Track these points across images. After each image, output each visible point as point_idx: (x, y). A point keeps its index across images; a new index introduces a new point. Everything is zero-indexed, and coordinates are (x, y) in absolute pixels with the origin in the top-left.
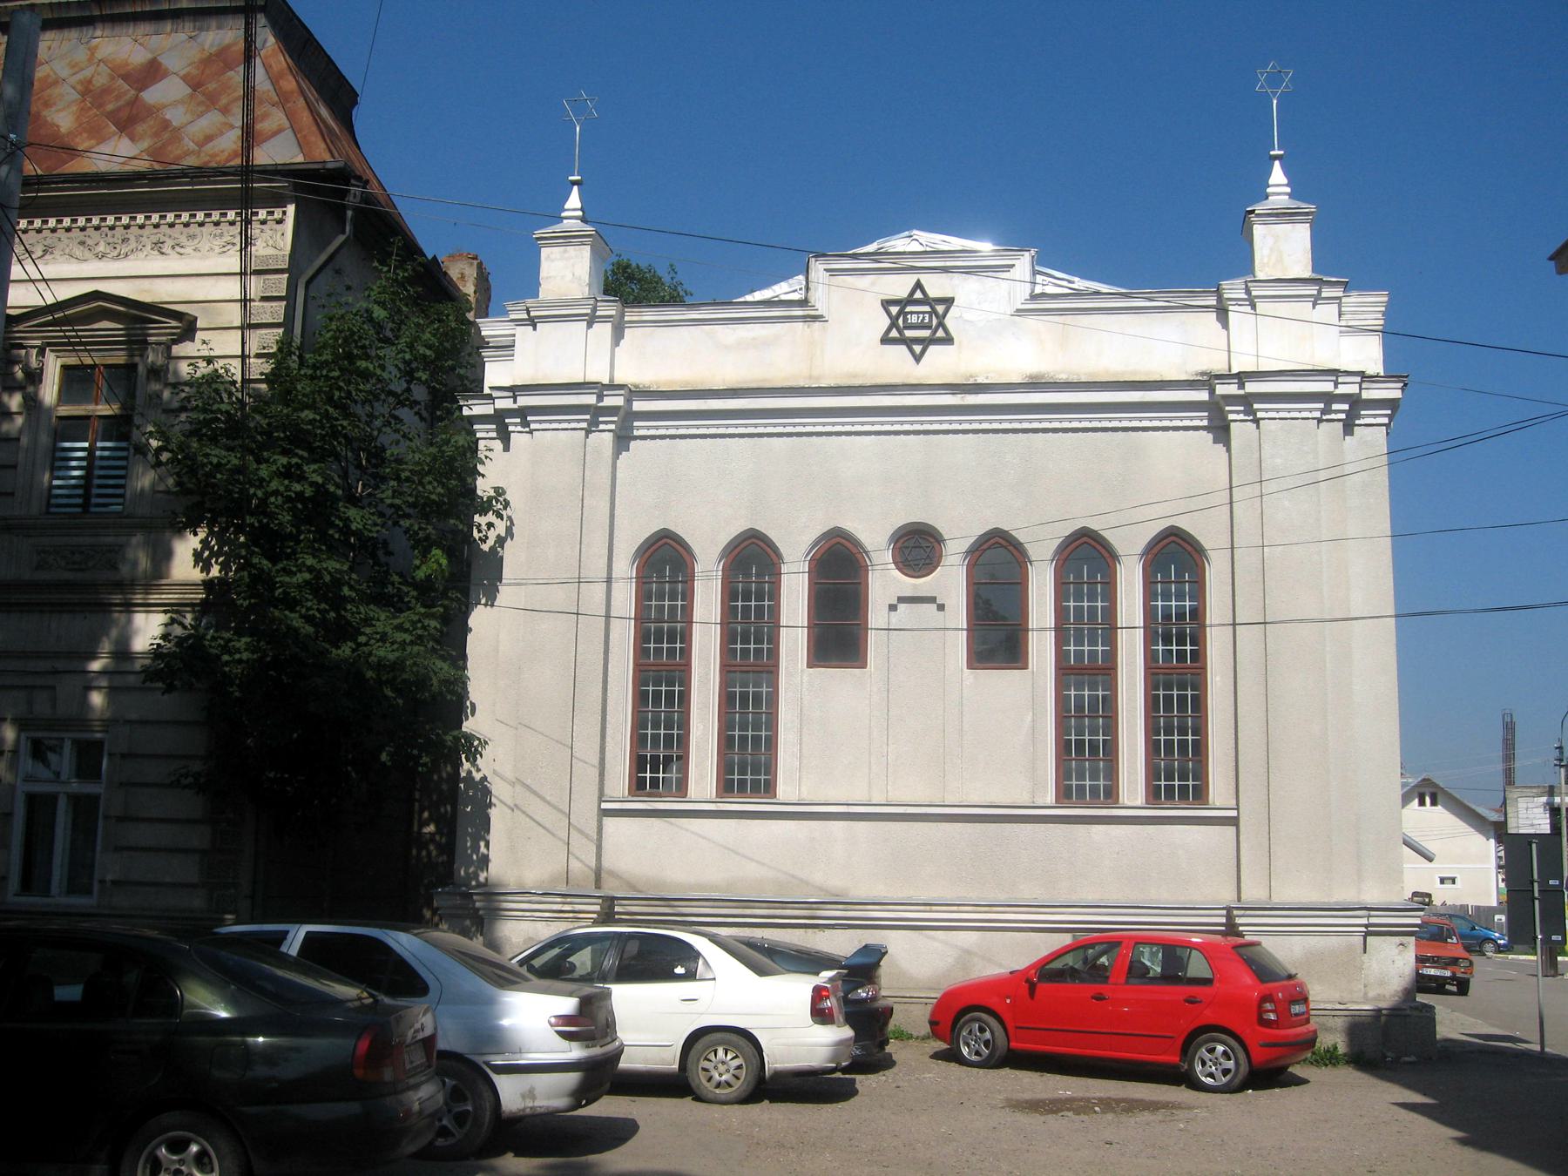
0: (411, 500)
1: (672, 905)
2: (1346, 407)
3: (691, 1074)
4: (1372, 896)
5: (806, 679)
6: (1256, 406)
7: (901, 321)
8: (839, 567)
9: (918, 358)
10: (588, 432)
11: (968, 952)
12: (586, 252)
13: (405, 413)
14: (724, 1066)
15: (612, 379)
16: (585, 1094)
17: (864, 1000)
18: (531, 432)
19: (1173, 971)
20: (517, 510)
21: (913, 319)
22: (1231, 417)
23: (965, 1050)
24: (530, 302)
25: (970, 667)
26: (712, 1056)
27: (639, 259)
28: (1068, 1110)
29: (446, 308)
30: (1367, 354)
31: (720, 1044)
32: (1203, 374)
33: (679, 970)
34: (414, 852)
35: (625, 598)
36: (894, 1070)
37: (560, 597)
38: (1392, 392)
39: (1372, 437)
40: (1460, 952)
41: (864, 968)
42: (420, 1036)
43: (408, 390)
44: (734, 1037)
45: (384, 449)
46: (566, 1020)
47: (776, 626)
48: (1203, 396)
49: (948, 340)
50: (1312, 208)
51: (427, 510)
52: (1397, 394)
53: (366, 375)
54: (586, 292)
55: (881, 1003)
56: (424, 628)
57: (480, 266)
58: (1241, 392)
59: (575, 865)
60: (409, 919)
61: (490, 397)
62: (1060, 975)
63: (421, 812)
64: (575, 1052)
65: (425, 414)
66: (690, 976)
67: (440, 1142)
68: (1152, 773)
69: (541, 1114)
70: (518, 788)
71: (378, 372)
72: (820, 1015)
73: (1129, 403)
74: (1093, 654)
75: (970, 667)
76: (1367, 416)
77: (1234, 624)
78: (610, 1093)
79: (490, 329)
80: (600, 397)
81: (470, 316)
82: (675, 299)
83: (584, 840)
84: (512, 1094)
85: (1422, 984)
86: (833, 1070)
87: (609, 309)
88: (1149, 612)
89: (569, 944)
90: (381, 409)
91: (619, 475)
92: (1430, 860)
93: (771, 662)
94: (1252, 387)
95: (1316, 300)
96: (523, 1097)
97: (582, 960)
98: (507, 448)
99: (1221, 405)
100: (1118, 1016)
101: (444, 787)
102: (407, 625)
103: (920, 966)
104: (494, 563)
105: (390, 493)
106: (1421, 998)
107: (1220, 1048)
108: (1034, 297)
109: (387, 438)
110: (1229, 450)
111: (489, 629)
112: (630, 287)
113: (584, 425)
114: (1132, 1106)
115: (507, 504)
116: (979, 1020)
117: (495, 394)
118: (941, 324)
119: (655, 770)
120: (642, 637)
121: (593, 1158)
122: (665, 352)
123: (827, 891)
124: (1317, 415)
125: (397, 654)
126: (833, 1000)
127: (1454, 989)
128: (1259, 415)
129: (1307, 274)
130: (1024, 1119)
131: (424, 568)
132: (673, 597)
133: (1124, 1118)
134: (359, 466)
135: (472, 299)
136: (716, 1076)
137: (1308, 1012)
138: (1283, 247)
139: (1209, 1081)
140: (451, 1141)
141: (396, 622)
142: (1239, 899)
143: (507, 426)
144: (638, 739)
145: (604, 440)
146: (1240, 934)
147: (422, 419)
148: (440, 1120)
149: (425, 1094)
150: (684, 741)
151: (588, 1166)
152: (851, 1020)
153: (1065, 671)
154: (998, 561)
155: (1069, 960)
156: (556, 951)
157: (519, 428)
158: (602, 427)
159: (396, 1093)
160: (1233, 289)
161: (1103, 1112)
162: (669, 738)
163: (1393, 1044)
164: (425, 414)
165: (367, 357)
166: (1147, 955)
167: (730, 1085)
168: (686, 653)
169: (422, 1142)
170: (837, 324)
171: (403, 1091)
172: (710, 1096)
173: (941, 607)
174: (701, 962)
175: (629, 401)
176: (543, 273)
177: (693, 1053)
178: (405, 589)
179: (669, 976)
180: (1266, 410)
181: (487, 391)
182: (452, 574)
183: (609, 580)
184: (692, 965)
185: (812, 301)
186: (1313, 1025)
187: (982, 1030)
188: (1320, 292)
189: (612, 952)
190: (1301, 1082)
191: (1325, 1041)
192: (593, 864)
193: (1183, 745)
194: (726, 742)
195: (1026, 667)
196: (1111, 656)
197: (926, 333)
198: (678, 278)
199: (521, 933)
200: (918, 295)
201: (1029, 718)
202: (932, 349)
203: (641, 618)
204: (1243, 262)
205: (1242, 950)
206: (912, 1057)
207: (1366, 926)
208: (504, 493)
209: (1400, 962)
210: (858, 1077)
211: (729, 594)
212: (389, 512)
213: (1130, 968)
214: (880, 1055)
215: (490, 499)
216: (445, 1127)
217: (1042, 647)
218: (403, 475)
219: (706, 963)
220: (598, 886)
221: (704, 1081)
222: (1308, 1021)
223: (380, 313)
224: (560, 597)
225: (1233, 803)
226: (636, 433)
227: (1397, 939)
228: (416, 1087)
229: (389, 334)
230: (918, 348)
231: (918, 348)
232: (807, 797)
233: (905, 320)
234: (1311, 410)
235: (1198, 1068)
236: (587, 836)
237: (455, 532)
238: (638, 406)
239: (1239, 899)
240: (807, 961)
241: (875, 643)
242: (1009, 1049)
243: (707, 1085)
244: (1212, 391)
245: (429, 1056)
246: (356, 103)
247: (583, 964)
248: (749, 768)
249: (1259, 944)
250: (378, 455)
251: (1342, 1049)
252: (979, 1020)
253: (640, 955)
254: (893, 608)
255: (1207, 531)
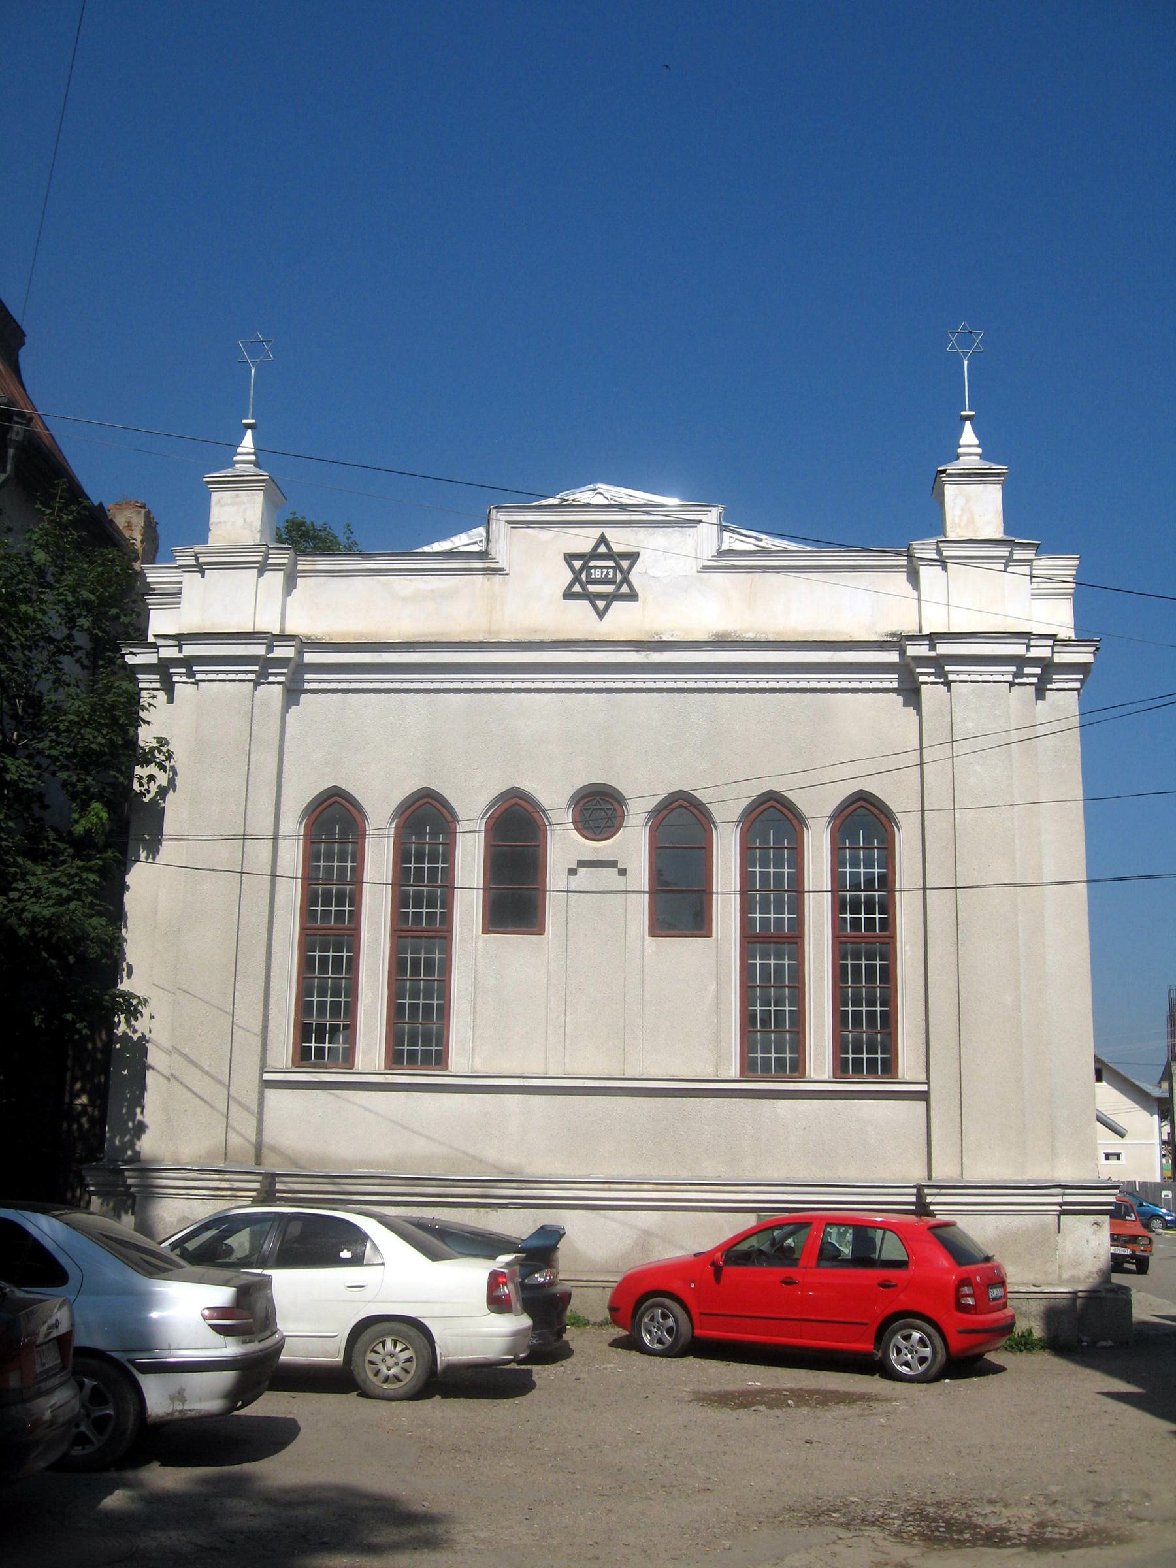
0: (69, 750)
1: (339, 1184)
2: (1038, 671)
3: (357, 1371)
4: (1066, 1173)
5: (480, 944)
6: (947, 668)
7: (584, 576)
8: (516, 831)
9: (601, 614)
10: (257, 684)
11: (647, 1233)
12: (259, 497)
13: (67, 662)
14: (392, 1359)
15: (282, 630)
16: (242, 1393)
17: (541, 1286)
18: (196, 683)
19: (864, 1256)
20: (179, 761)
21: (597, 574)
22: (922, 679)
23: (647, 1339)
24: (198, 548)
25: (653, 933)
26: (379, 1348)
27: (314, 517)
28: (760, 1403)
29: (112, 553)
30: (1059, 617)
31: (388, 1335)
32: (893, 635)
33: (346, 1254)
34: (65, 1125)
35: (292, 856)
36: (573, 1359)
37: (224, 854)
38: (1084, 656)
39: (1064, 701)
40: (1139, 1230)
41: (541, 1250)
42: (55, 1334)
43: (70, 637)
44: (404, 1328)
45: (41, 699)
46: (221, 1312)
47: (449, 887)
48: (894, 657)
49: (633, 596)
50: (1004, 469)
51: (87, 760)
52: (1089, 658)
53: (26, 620)
54: (256, 538)
55: (559, 1289)
56: (82, 882)
57: (148, 515)
58: (933, 654)
59: (235, 1140)
60: (57, 1195)
61: (153, 645)
62: (746, 1258)
63: (74, 1082)
64: (230, 1349)
65: (86, 662)
66: (357, 1260)
67: (77, 1451)
68: (840, 1045)
69: (193, 1419)
70: (175, 1056)
71: (39, 616)
72: (497, 1303)
73: (822, 663)
74: (779, 922)
75: (653, 933)
76: (1059, 681)
77: (925, 889)
78: (269, 1389)
79: (156, 575)
80: (270, 648)
81: (137, 566)
82: (350, 550)
83: (245, 1114)
84: (158, 1397)
85: (1117, 1264)
86: (509, 1362)
87: (281, 557)
88: (837, 878)
89: (225, 1225)
90: (40, 657)
91: (287, 730)
92: (1122, 1136)
93: (352, 926)
94: (943, 649)
95: (1008, 561)
96: (172, 1399)
97: (240, 1242)
98: (170, 700)
99: (913, 668)
100: (816, 1302)
101: (99, 1056)
102: (64, 879)
103: (597, 1248)
104: (155, 815)
105: (47, 743)
106: (1117, 1279)
107: (916, 1335)
108: (721, 553)
109: (44, 685)
110: (919, 713)
111: (147, 885)
112: (302, 538)
113: (253, 677)
114: (827, 1398)
115: (170, 756)
116: (660, 1305)
117: (160, 642)
118: (625, 580)
119: (320, 1040)
120: (310, 899)
121: (248, 1467)
122: (337, 604)
123: (502, 1171)
124: (1009, 678)
125: (52, 910)
126: (511, 1286)
127: (1134, 1267)
128: (951, 677)
129: (999, 535)
130: (715, 1415)
131: (83, 821)
132: (342, 859)
133: (819, 1412)
134: (15, 716)
135: (138, 546)
136: (384, 1370)
137: (1005, 1296)
138: (974, 509)
139: (904, 1370)
140: (89, 1449)
141: (50, 876)
142: (930, 1178)
143: (171, 675)
144: (304, 1007)
145: (273, 693)
146: (932, 1214)
147: (83, 667)
148: (77, 1426)
149: (58, 1401)
150: (351, 1009)
151: (246, 1479)
152: (529, 1307)
153: (751, 940)
154: (681, 827)
155: (753, 1242)
156: (211, 1233)
157: (184, 679)
158: (271, 679)
159: (24, 1401)
160: (925, 548)
161: (797, 1406)
162: (336, 1006)
163: (1091, 1328)
164: (86, 662)
165: (28, 600)
166: (834, 1236)
167: (399, 1380)
168: (355, 916)
169: (55, 1455)
170: (520, 576)
171: (31, 1399)
172: (378, 1392)
173: (623, 872)
174: (368, 1245)
175: (300, 653)
176: (213, 519)
177: (358, 1345)
178: (61, 846)
179: (330, 1259)
180: (958, 673)
181: (151, 639)
182: (111, 831)
183: (276, 838)
184: (360, 1248)
185: (492, 552)
186: (1009, 1311)
187: (665, 1316)
188: (1011, 553)
189: (273, 1234)
190: (998, 1369)
191: (1021, 1326)
192: (253, 1137)
193: (871, 1015)
194: (396, 1011)
195: (709, 935)
196: (798, 924)
197: (610, 589)
198: (354, 538)
199: (178, 1213)
200: (602, 549)
201: (714, 987)
202: (616, 604)
203: (309, 878)
204: (935, 523)
205: (938, 1231)
206: (589, 1343)
207: (1060, 1204)
208: (167, 743)
209: (1094, 1243)
210: (536, 1369)
211: (402, 855)
212: (45, 763)
213: (821, 1250)
214: (557, 1344)
215: (152, 749)
216: (82, 1434)
217: (726, 912)
218: (62, 727)
219: (374, 1246)
220: (258, 1160)
221: (371, 1375)
222: (1005, 1306)
223: (40, 557)
224: (224, 854)
225: (923, 1078)
226: (307, 686)
227: (1092, 1218)
228: (49, 1392)
229: (50, 579)
230: (601, 603)
231: (601, 604)
232: (480, 1068)
233: (589, 574)
234: (1003, 673)
235: (893, 1356)
236: (247, 1109)
237: (114, 785)
238: (310, 658)
239: (930, 1178)
240: (482, 1244)
241: (553, 905)
242: (693, 1336)
243: (374, 1379)
244: (903, 653)
245: (64, 1357)
246: (144, 1132)
247: (241, 1245)
248: (420, 1036)
249: (953, 1224)
250: (35, 703)
251: (1038, 1333)
252: (660, 1305)
253: (302, 1238)
254: (572, 872)
255: (898, 796)
